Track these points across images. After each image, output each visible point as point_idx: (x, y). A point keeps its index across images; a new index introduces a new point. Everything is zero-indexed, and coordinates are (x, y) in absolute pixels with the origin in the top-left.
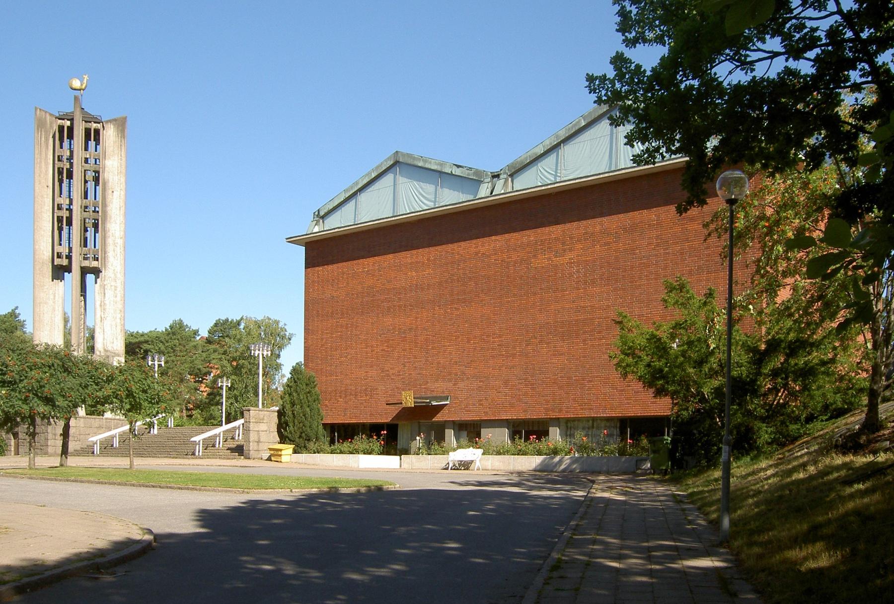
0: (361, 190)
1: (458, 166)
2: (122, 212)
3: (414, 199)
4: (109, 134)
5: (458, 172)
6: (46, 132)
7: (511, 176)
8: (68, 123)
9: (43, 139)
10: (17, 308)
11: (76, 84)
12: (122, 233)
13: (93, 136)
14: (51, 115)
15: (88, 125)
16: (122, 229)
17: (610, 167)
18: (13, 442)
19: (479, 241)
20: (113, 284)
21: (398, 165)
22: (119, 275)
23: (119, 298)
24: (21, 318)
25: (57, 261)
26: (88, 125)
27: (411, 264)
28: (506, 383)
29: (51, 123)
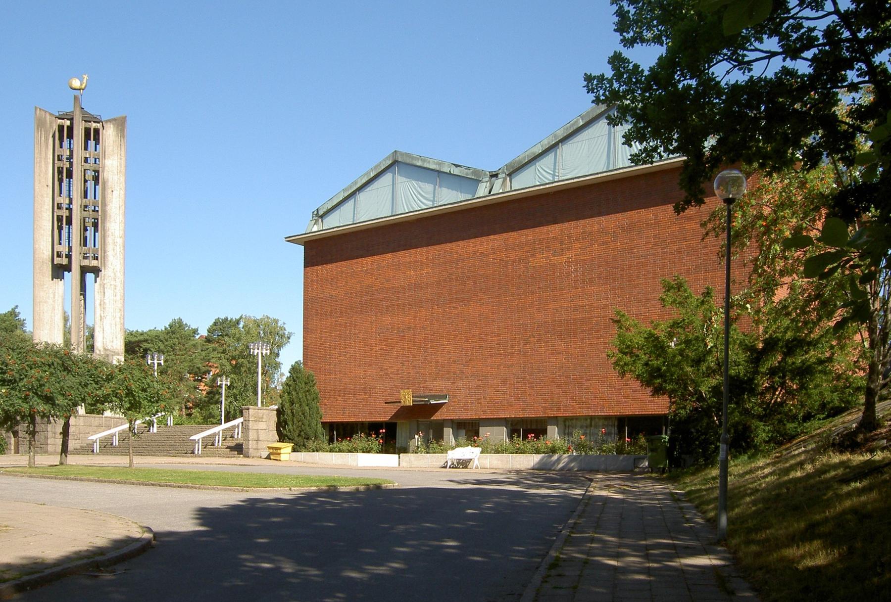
0: (360, 189)
1: (457, 166)
2: (122, 211)
3: (413, 198)
4: (109, 134)
5: (456, 171)
6: (46, 131)
7: (510, 175)
8: (68, 123)
9: (43, 138)
10: (17, 307)
11: (76, 83)
12: (122, 232)
13: (93, 136)
14: (51, 114)
15: (88, 125)
16: (122, 228)
17: (608, 166)
18: (13, 440)
19: (478, 241)
20: (113, 283)
21: (396, 164)
22: (118, 275)
23: (118, 297)
24: (21, 317)
25: (57, 261)
26: (88, 125)
27: (409, 263)
28: (504, 381)
29: (51, 123)
